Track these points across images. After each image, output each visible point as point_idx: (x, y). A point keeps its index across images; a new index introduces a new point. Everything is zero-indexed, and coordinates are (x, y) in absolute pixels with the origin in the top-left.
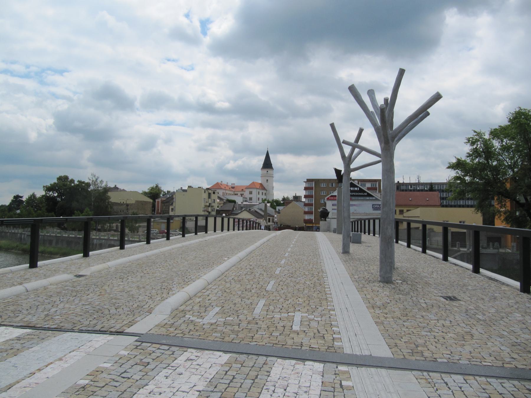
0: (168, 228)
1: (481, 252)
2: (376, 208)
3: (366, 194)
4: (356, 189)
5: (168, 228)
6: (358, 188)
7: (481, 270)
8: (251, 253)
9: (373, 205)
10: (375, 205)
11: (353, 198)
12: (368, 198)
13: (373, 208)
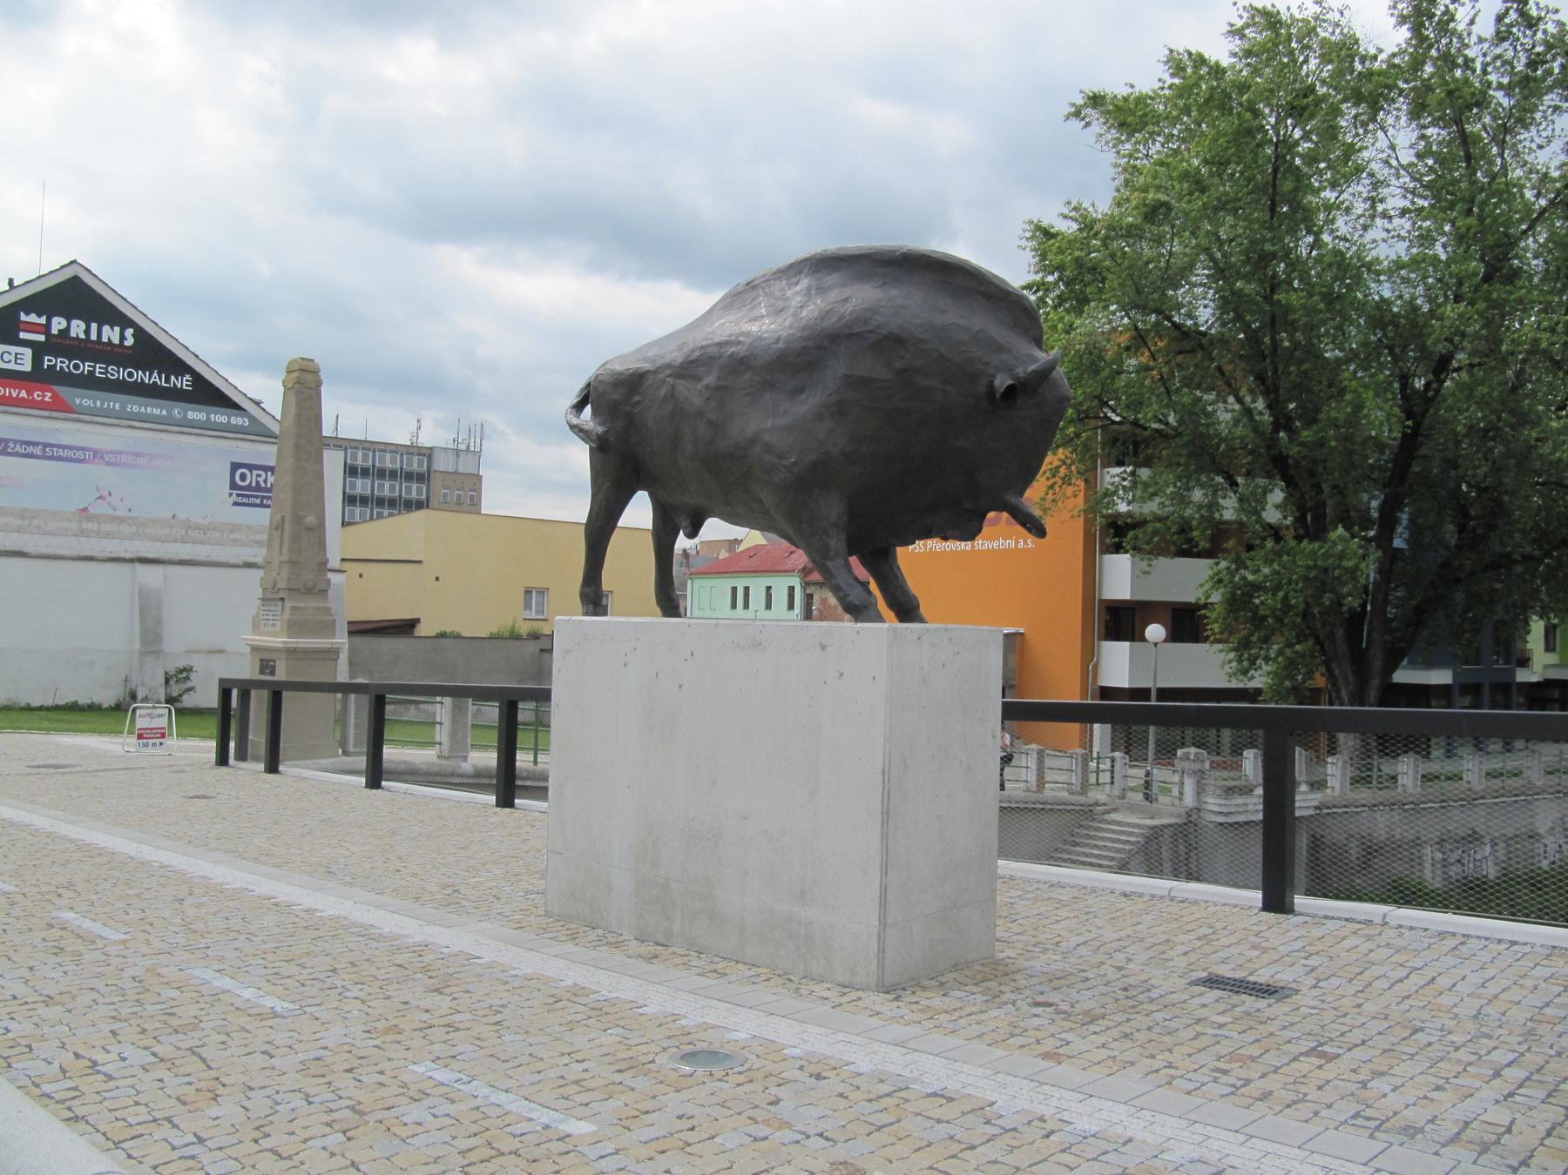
0: (536, 743)
1: (1298, 813)
2: (258, 488)
3: (184, 382)
4: (111, 334)
5: (536, 743)
6: (129, 332)
7: (1300, 901)
8: (13, 824)
9: (235, 467)
10: (251, 467)
11: (87, 402)
12: (196, 414)
13: (233, 486)
